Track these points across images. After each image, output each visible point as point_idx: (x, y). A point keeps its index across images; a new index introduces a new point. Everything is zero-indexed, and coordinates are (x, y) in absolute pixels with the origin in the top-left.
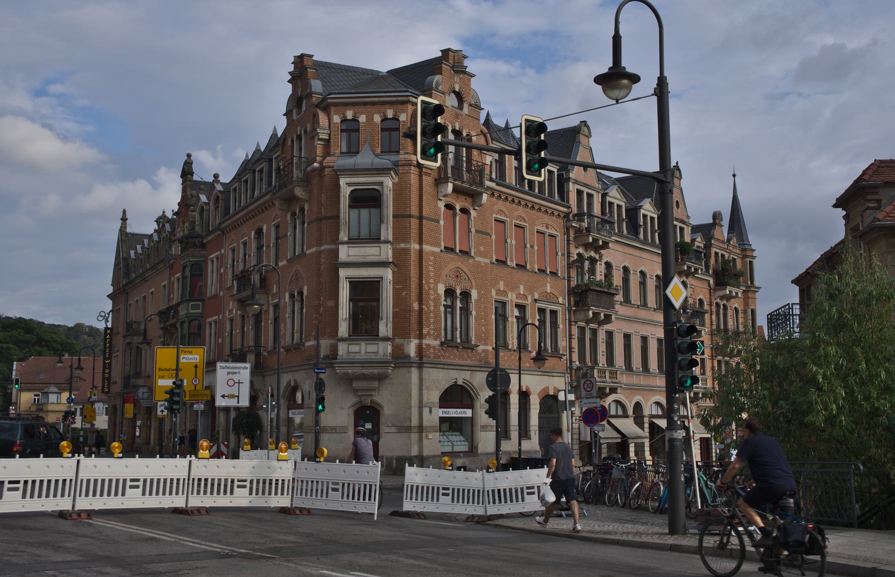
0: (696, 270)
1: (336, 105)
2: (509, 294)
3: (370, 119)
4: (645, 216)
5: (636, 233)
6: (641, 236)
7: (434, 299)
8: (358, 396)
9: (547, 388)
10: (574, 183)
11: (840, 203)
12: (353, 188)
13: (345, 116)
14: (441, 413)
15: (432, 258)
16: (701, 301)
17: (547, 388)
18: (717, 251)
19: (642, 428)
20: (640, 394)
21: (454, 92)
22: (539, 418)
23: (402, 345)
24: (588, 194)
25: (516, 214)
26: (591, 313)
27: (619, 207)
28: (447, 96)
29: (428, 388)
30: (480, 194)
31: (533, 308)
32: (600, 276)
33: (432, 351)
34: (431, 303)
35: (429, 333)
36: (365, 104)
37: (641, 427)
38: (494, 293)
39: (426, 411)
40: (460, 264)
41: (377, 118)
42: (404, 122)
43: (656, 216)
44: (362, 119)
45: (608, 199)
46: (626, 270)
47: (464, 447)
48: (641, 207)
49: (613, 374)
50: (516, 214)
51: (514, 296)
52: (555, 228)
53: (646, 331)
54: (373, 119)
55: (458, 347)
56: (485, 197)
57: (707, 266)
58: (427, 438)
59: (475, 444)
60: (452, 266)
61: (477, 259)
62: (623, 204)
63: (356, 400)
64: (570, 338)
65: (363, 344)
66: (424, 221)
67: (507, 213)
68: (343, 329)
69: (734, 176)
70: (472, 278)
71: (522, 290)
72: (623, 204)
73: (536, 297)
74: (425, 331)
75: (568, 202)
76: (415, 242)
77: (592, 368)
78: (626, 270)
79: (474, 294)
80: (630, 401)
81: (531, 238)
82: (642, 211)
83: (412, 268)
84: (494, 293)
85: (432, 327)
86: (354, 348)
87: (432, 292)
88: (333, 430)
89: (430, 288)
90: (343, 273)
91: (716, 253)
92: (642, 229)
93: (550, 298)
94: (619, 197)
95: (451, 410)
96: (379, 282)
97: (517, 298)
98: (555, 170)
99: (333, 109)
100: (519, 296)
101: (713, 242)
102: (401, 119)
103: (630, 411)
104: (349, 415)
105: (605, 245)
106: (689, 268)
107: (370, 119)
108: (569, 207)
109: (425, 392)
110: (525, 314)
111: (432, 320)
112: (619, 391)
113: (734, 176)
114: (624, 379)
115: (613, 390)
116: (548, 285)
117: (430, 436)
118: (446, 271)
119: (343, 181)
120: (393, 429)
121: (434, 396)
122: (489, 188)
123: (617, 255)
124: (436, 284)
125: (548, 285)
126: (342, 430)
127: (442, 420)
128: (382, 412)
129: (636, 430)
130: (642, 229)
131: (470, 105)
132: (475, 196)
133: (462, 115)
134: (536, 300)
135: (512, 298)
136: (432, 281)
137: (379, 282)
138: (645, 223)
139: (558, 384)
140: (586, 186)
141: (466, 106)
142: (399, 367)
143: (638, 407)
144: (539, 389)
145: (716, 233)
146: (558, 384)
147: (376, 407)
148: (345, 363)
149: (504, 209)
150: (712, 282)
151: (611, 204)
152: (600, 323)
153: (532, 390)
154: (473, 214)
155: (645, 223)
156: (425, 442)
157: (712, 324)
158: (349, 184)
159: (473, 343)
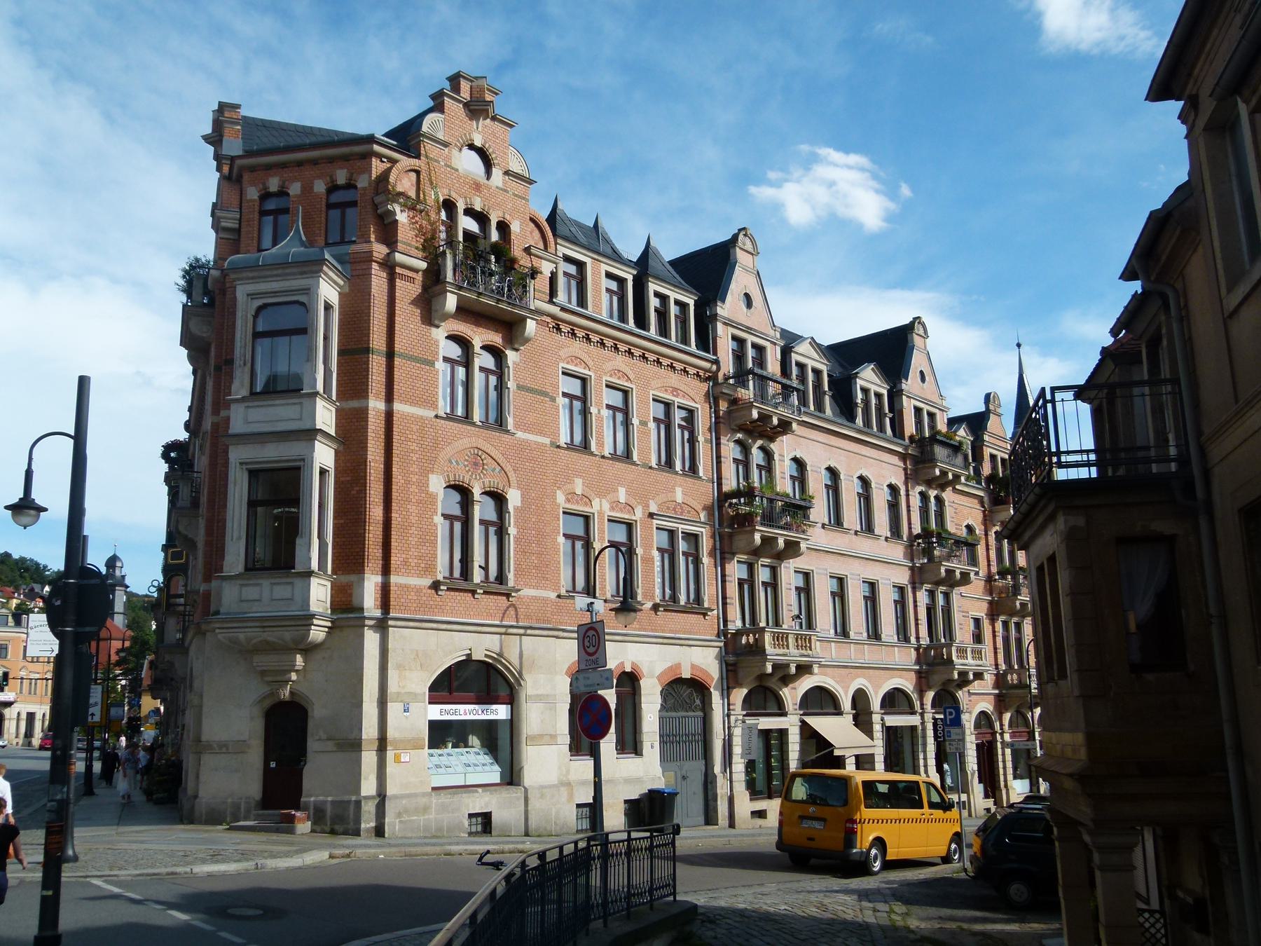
1: (253, 169)
2: (596, 502)
3: (307, 189)
4: (865, 391)
5: (851, 417)
7: (419, 502)
8: (268, 683)
9: (678, 666)
10: (725, 324)
11: (1161, 90)
13: (266, 188)
14: (437, 712)
15: (415, 428)
16: (969, 528)
17: (678, 666)
19: (869, 732)
21: (472, 147)
25: (609, 366)
26: (757, 537)
27: (817, 372)
28: (455, 152)
29: (400, 667)
30: (523, 320)
31: (647, 528)
33: (412, 596)
34: (413, 508)
35: (405, 562)
36: (300, 164)
37: (869, 732)
38: (561, 498)
39: (394, 709)
41: (320, 187)
42: (364, 189)
44: (295, 189)
46: (833, 472)
49: (804, 642)
50: (609, 366)
53: (873, 572)
54: (312, 188)
55: (473, 592)
56: (531, 326)
58: (397, 759)
60: (465, 443)
61: (520, 434)
62: (824, 368)
63: (265, 690)
66: (397, 361)
67: (590, 363)
69: (1019, 345)
70: (508, 468)
71: (622, 495)
72: (824, 368)
74: (394, 560)
75: (715, 353)
76: (377, 397)
77: (949, 646)
78: (833, 472)
79: (514, 498)
80: (846, 689)
81: (645, 413)
82: (859, 382)
84: (561, 498)
85: (414, 552)
86: (251, 592)
88: (223, 747)
89: (408, 482)
90: (237, 455)
91: (993, 457)
92: (860, 410)
95: (462, 707)
96: (299, 468)
97: (612, 509)
100: (615, 504)
101: (986, 438)
103: (846, 704)
104: (252, 718)
105: (785, 427)
106: (944, 473)
107: (307, 189)
108: (717, 362)
110: (697, 549)
111: (413, 540)
112: (816, 669)
113: (1019, 345)
115: (804, 669)
116: (679, 491)
117: (405, 757)
118: (447, 452)
120: (330, 745)
121: (421, 682)
122: (538, 312)
123: (810, 448)
124: (425, 473)
125: (679, 491)
127: (434, 725)
129: (859, 737)
131: (507, 173)
132: (511, 328)
133: (489, 188)
134: (651, 515)
135: (600, 508)
136: (414, 468)
137: (299, 468)
138: (866, 402)
140: (749, 330)
141: (497, 173)
144: (660, 668)
147: (303, 703)
150: (986, 499)
151: (802, 367)
152: (781, 556)
153: (644, 670)
155: (866, 402)
156: (391, 768)
157: (989, 565)
158: (252, 296)
159: (706, 605)
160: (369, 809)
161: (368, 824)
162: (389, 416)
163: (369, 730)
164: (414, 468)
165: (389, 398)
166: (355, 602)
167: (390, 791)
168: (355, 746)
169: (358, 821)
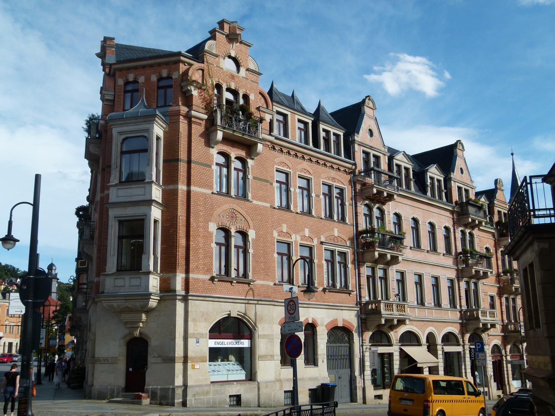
0: (480, 223)
1: (120, 70)
2: (293, 236)
3: (148, 79)
4: (432, 178)
5: (425, 192)
6: (429, 194)
7: (204, 236)
8: (129, 328)
10: (359, 145)
12: (124, 136)
13: (127, 79)
14: (213, 343)
15: (202, 199)
18: (500, 210)
20: (432, 326)
21: (230, 57)
22: (328, 347)
23: (169, 279)
24: (374, 156)
25: (300, 167)
27: (407, 169)
28: (221, 60)
29: (194, 320)
30: (256, 144)
31: (320, 250)
32: (390, 227)
34: (201, 240)
35: (197, 267)
36: (144, 67)
37: (435, 355)
38: (275, 234)
39: (191, 342)
40: (235, 207)
41: (154, 78)
43: (442, 179)
44: (141, 79)
45: (395, 161)
47: (242, 375)
48: (427, 171)
49: (401, 308)
50: (300, 167)
51: (299, 238)
52: (342, 181)
53: (437, 272)
54: (150, 79)
55: (231, 282)
56: (260, 147)
57: (491, 220)
58: (193, 367)
59: (253, 372)
60: (226, 206)
63: (127, 331)
64: (502, 314)
65: (127, 278)
66: (193, 165)
67: (290, 165)
68: (112, 265)
69: (512, 154)
70: (249, 219)
71: (307, 232)
73: (323, 239)
74: (191, 266)
75: (354, 160)
76: (183, 183)
79: (252, 234)
81: (318, 190)
82: (429, 174)
83: (180, 207)
84: (275, 234)
85: (201, 262)
86: (120, 282)
87: (201, 230)
88: (106, 361)
89: (198, 226)
90: (113, 213)
92: (429, 189)
93: (335, 241)
94: (406, 161)
96: (143, 220)
98: (342, 134)
99: (117, 74)
100: (303, 237)
101: (496, 202)
102: (174, 77)
103: (424, 340)
105: (390, 197)
107: (148, 79)
108: (355, 164)
109: (190, 323)
113: (512, 154)
114: (417, 313)
115: (401, 322)
117: (197, 366)
118: (218, 211)
119: (115, 131)
120: (159, 360)
121: (205, 328)
122: (264, 140)
124: (207, 222)
126: (113, 361)
127: (211, 350)
128: (149, 344)
129: (430, 358)
130: (429, 189)
131: (248, 70)
134: (322, 243)
135: (296, 239)
137: (143, 220)
138: (432, 184)
139: (349, 317)
140: (371, 148)
142: (165, 300)
143: (431, 337)
144: (327, 321)
145: (499, 195)
146: (349, 317)
147: (146, 338)
148: (110, 296)
149: (288, 163)
151: (399, 166)
152: (389, 264)
153: (319, 322)
154: (250, 162)
156: (190, 371)
157: (498, 268)
158: (120, 133)
160: (179, 392)
161: (178, 400)
162: (189, 193)
163: (179, 352)
164: (201, 219)
165: (189, 184)
166: (172, 288)
167: (190, 383)
168: (172, 360)
169: (173, 398)
